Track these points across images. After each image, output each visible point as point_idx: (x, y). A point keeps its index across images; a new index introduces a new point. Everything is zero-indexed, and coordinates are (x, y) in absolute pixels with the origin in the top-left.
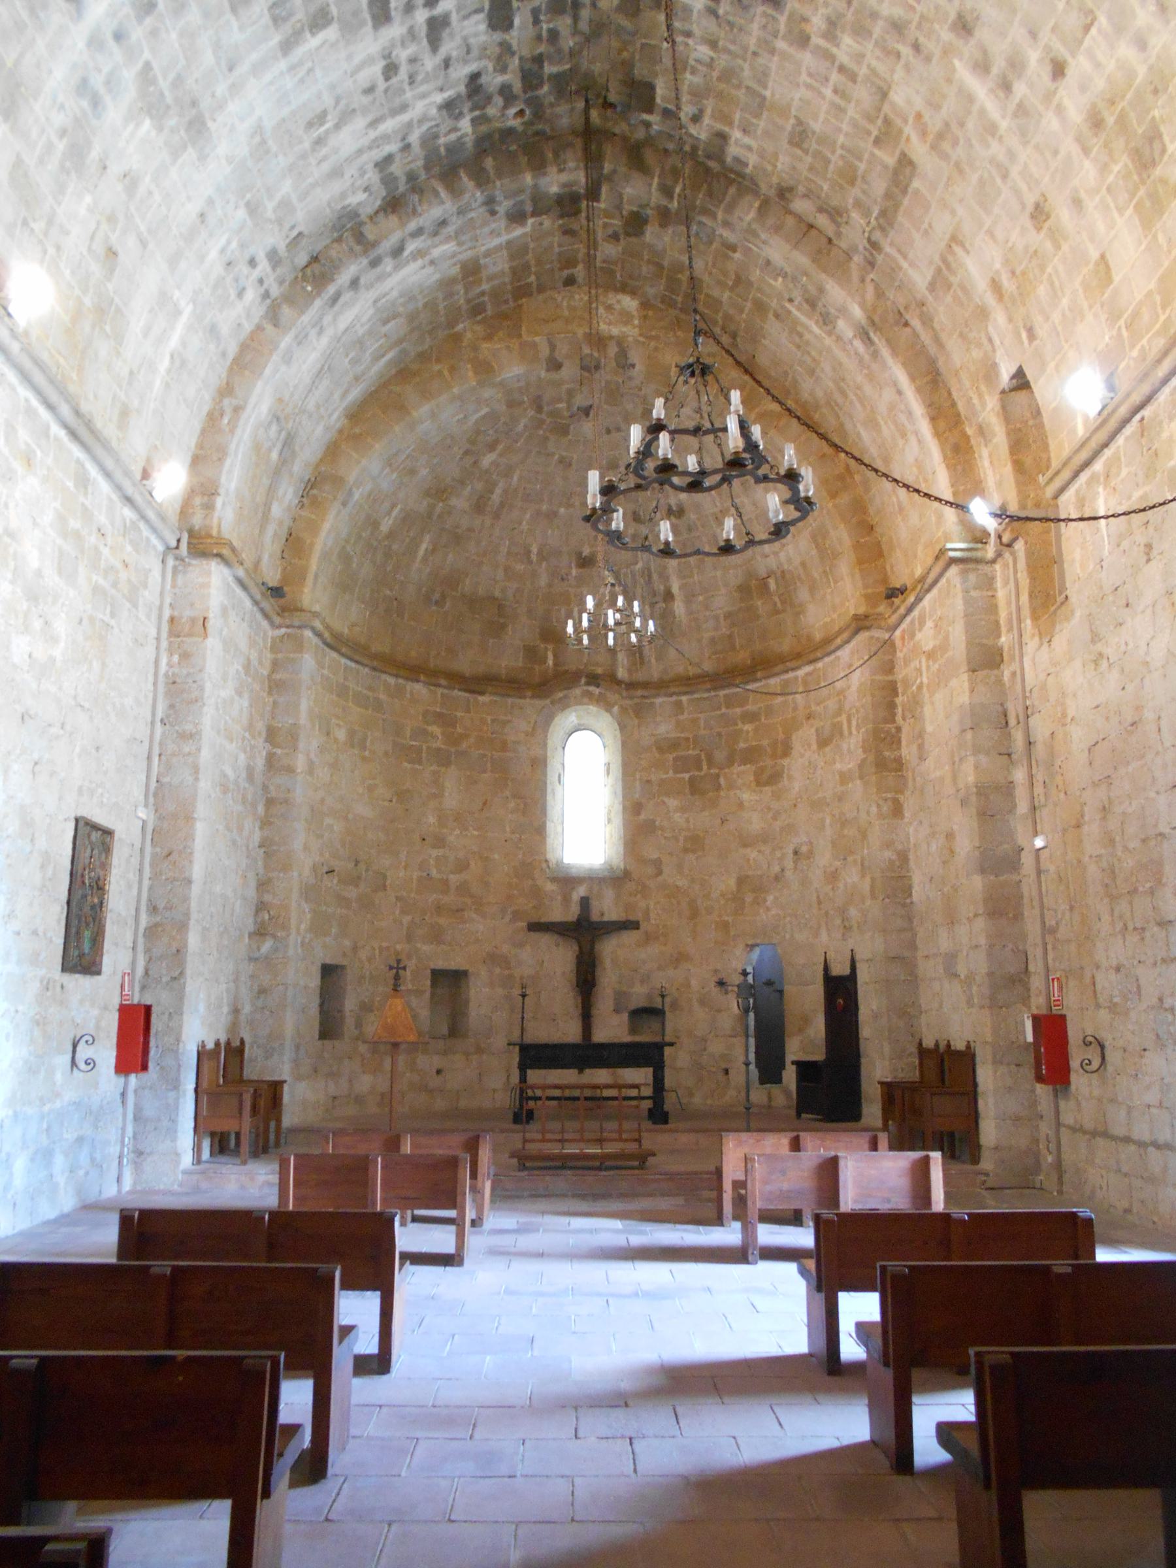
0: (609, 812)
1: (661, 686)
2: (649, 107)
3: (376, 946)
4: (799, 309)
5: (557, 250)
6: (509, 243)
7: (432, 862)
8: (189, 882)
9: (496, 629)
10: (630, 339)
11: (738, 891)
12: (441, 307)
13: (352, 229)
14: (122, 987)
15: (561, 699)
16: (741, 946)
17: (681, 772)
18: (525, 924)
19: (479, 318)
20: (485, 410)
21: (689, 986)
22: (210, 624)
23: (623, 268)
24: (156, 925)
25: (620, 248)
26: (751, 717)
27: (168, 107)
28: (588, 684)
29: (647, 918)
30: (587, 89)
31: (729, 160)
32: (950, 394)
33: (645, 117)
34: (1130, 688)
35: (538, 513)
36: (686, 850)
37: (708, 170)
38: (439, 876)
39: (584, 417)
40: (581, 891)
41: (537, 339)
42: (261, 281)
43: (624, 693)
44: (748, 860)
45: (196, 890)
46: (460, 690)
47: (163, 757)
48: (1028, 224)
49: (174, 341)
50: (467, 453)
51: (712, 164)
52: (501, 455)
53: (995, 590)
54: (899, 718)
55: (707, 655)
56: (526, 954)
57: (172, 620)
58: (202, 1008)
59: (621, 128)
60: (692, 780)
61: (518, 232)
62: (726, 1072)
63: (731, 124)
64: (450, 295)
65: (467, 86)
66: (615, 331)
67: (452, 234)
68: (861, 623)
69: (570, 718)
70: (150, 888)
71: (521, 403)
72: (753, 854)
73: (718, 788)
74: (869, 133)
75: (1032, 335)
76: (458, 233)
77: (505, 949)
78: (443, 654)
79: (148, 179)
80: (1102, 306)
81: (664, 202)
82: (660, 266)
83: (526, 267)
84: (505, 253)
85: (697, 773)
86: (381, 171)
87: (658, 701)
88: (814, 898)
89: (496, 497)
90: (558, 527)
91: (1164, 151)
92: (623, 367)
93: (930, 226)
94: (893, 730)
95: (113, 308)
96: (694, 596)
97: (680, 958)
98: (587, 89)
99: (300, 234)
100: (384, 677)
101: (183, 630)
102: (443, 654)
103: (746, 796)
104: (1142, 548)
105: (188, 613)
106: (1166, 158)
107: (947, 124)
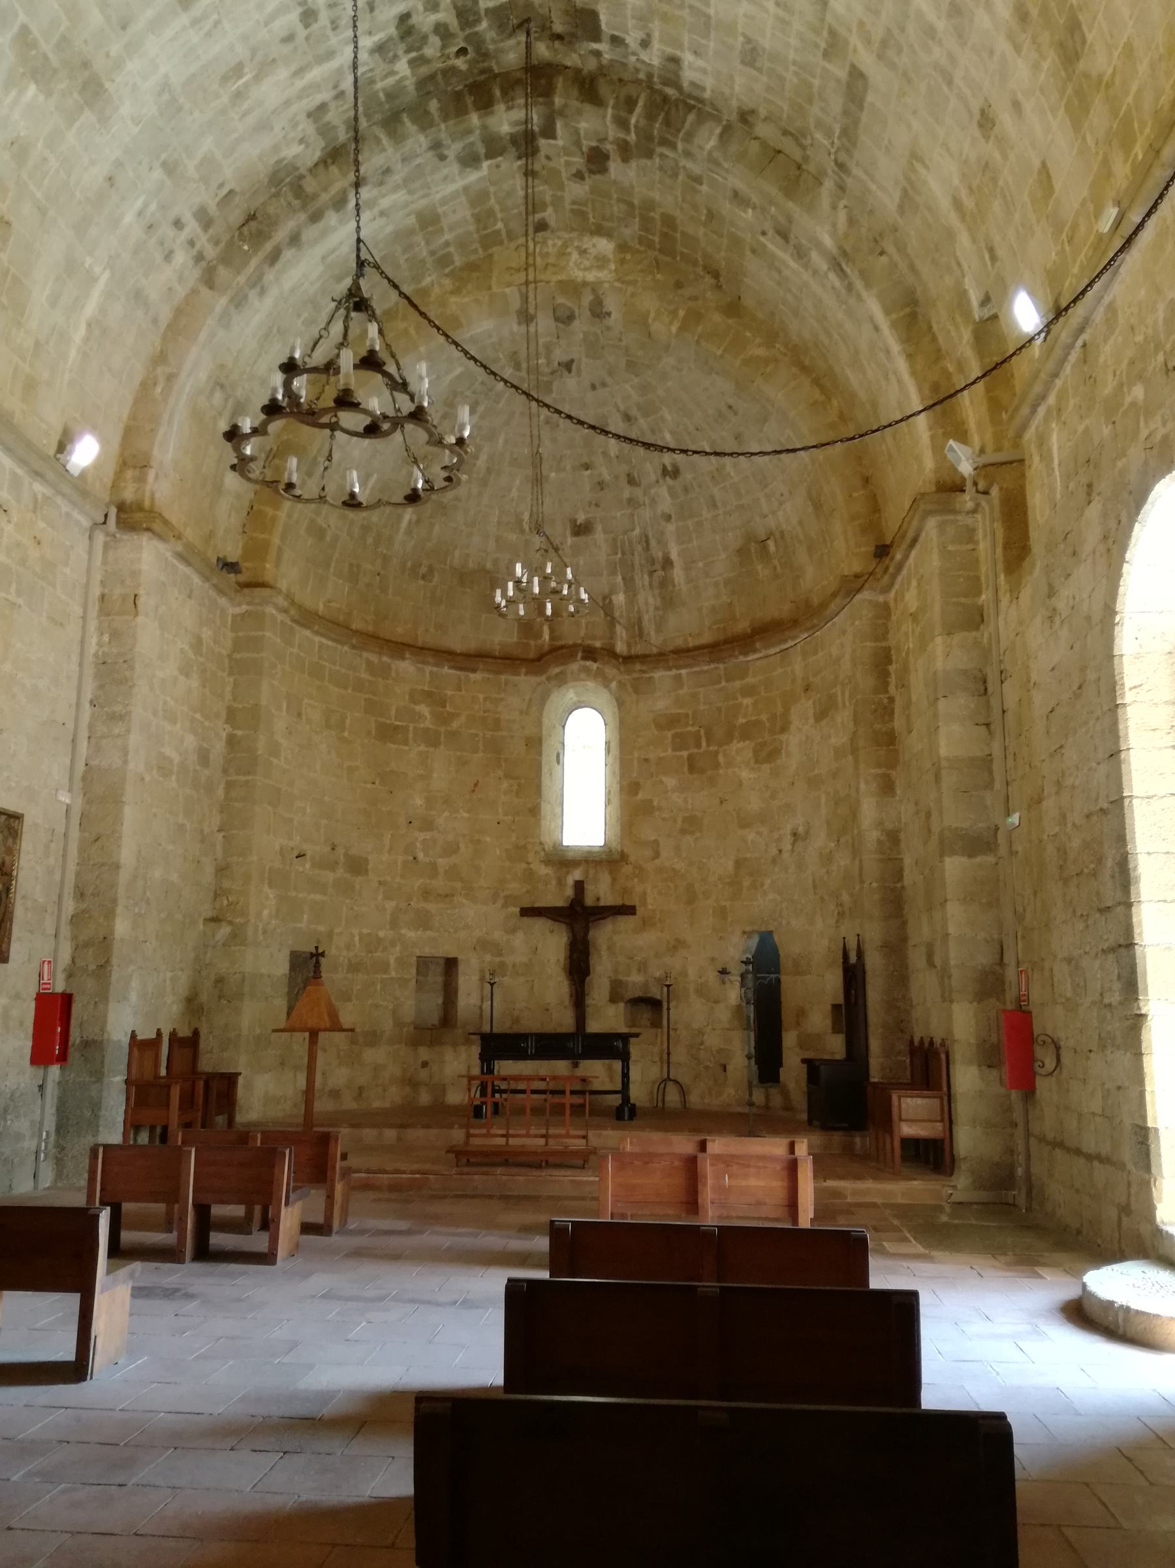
1: (660, 658)
2: (596, 36)
3: (355, 931)
6: (466, 189)
7: (418, 845)
8: (117, 867)
10: (606, 285)
12: (402, 261)
13: (291, 183)
14: (41, 975)
15: (557, 675)
17: (680, 750)
19: (447, 271)
21: (686, 975)
22: (141, 601)
23: (594, 210)
24: (84, 911)
25: (587, 187)
26: (749, 691)
27: (55, 71)
28: (584, 658)
29: (644, 903)
30: (528, 20)
31: (685, 85)
32: (930, 328)
33: (595, 46)
34: (1077, 647)
36: (683, 832)
37: (666, 99)
38: (427, 860)
39: (566, 373)
40: (577, 875)
41: (507, 290)
42: (192, 243)
43: (622, 668)
45: (124, 877)
46: (450, 668)
47: (93, 740)
48: (977, 133)
49: (90, 309)
51: (670, 91)
53: (977, 543)
54: (892, 689)
56: (518, 940)
57: (103, 597)
58: (133, 997)
59: (572, 60)
60: (691, 760)
61: (473, 176)
62: (725, 1068)
63: (681, 47)
64: (408, 248)
65: (397, 28)
66: (591, 277)
67: (400, 182)
68: (852, 585)
69: (570, 694)
70: (78, 874)
72: (751, 836)
73: (717, 766)
74: (817, 46)
75: (994, 258)
76: (406, 181)
77: (498, 935)
78: (432, 630)
79: (40, 145)
80: (1047, 217)
81: (622, 135)
82: (631, 205)
83: (490, 213)
84: (463, 198)
85: (696, 751)
86: (315, 122)
87: (658, 674)
88: (810, 881)
91: (1084, 41)
92: (598, 316)
93: (890, 141)
94: (886, 701)
95: (9, 278)
96: (693, 562)
97: (678, 945)
98: (528, 20)
99: (231, 192)
100: (365, 654)
101: (116, 606)
102: (432, 630)
103: (745, 774)
104: (1085, 488)
105: (118, 591)
106: (1087, 47)
107: (889, 30)
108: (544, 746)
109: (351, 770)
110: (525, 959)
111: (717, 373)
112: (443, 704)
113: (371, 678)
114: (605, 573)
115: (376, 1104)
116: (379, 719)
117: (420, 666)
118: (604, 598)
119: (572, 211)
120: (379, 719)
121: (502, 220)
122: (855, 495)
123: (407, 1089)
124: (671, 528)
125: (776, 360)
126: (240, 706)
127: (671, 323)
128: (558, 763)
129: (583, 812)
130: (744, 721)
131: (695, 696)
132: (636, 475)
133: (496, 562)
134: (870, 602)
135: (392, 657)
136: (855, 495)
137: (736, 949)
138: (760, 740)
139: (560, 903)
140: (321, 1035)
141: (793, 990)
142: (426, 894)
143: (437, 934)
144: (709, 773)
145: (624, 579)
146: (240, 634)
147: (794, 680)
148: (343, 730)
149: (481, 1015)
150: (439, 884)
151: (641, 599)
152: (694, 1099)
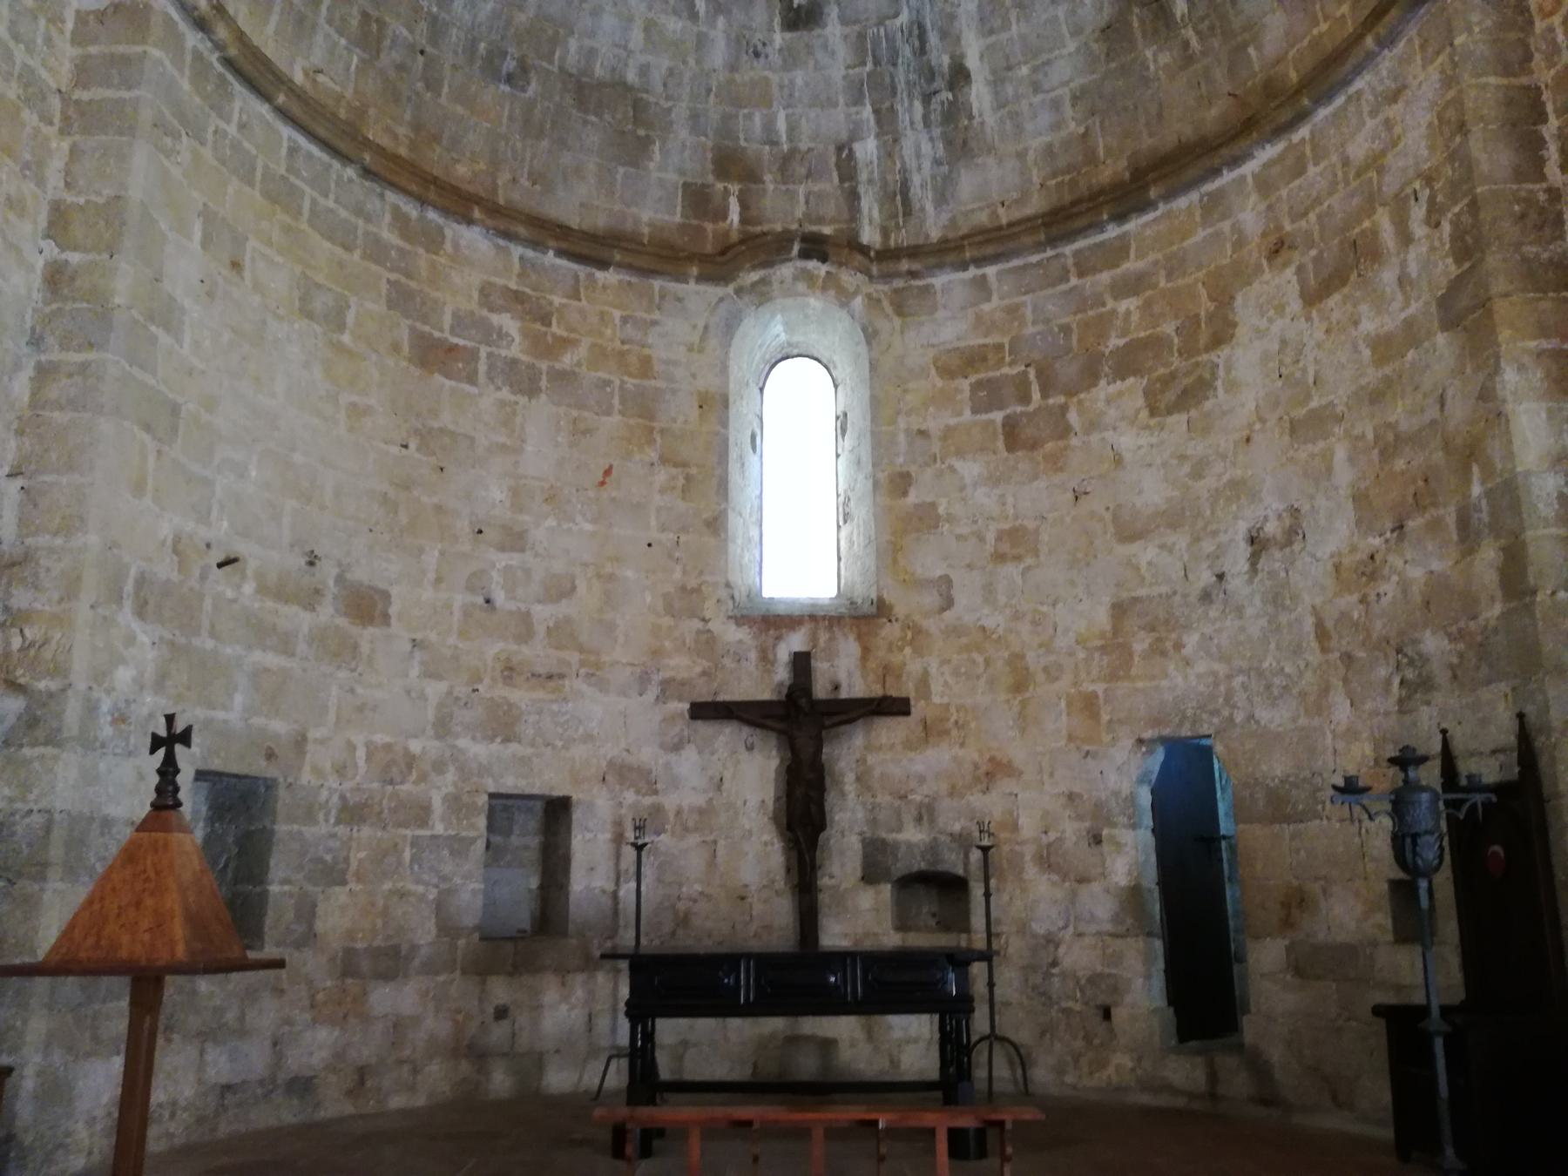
3: (359, 740)
7: (494, 574)
11: (1116, 631)
15: (754, 285)
16: (1128, 742)
17: (988, 410)
18: (687, 706)
21: (1015, 827)
28: (805, 255)
36: (999, 557)
38: (512, 606)
40: (796, 641)
46: (560, 253)
55: (1036, 180)
56: (688, 763)
62: (1107, 1014)
69: (772, 327)
72: (1146, 553)
73: (1065, 431)
77: (648, 755)
85: (1019, 409)
87: (939, 280)
88: (1309, 623)
94: (1542, 197)
96: (1009, 68)
97: (994, 771)
100: (392, 197)
103: (1127, 441)
108: (732, 411)
109: (356, 412)
110: (700, 800)
112: (545, 320)
113: (401, 243)
114: (841, 101)
115: (396, 1102)
116: (419, 325)
117: (501, 242)
118: (840, 149)
120: (419, 325)
123: (465, 1067)
126: (82, 200)
128: (754, 448)
129: (799, 532)
130: (1121, 342)
131: (1013, 311)
135: (446, 212)
137: (1126, 774)
138: (1162, 371)
139: (766, 695)
140: (172, 983)
141: (1262, 855)
142: (509, 672)
143: (529, 751)
144: (1050, 446)
145: (876, 112)
146: (93, 50)
147: (1240, 243)
148: (341, 327)
149: (616, 912)
150: (537, 654)
152: (1042, 1075)
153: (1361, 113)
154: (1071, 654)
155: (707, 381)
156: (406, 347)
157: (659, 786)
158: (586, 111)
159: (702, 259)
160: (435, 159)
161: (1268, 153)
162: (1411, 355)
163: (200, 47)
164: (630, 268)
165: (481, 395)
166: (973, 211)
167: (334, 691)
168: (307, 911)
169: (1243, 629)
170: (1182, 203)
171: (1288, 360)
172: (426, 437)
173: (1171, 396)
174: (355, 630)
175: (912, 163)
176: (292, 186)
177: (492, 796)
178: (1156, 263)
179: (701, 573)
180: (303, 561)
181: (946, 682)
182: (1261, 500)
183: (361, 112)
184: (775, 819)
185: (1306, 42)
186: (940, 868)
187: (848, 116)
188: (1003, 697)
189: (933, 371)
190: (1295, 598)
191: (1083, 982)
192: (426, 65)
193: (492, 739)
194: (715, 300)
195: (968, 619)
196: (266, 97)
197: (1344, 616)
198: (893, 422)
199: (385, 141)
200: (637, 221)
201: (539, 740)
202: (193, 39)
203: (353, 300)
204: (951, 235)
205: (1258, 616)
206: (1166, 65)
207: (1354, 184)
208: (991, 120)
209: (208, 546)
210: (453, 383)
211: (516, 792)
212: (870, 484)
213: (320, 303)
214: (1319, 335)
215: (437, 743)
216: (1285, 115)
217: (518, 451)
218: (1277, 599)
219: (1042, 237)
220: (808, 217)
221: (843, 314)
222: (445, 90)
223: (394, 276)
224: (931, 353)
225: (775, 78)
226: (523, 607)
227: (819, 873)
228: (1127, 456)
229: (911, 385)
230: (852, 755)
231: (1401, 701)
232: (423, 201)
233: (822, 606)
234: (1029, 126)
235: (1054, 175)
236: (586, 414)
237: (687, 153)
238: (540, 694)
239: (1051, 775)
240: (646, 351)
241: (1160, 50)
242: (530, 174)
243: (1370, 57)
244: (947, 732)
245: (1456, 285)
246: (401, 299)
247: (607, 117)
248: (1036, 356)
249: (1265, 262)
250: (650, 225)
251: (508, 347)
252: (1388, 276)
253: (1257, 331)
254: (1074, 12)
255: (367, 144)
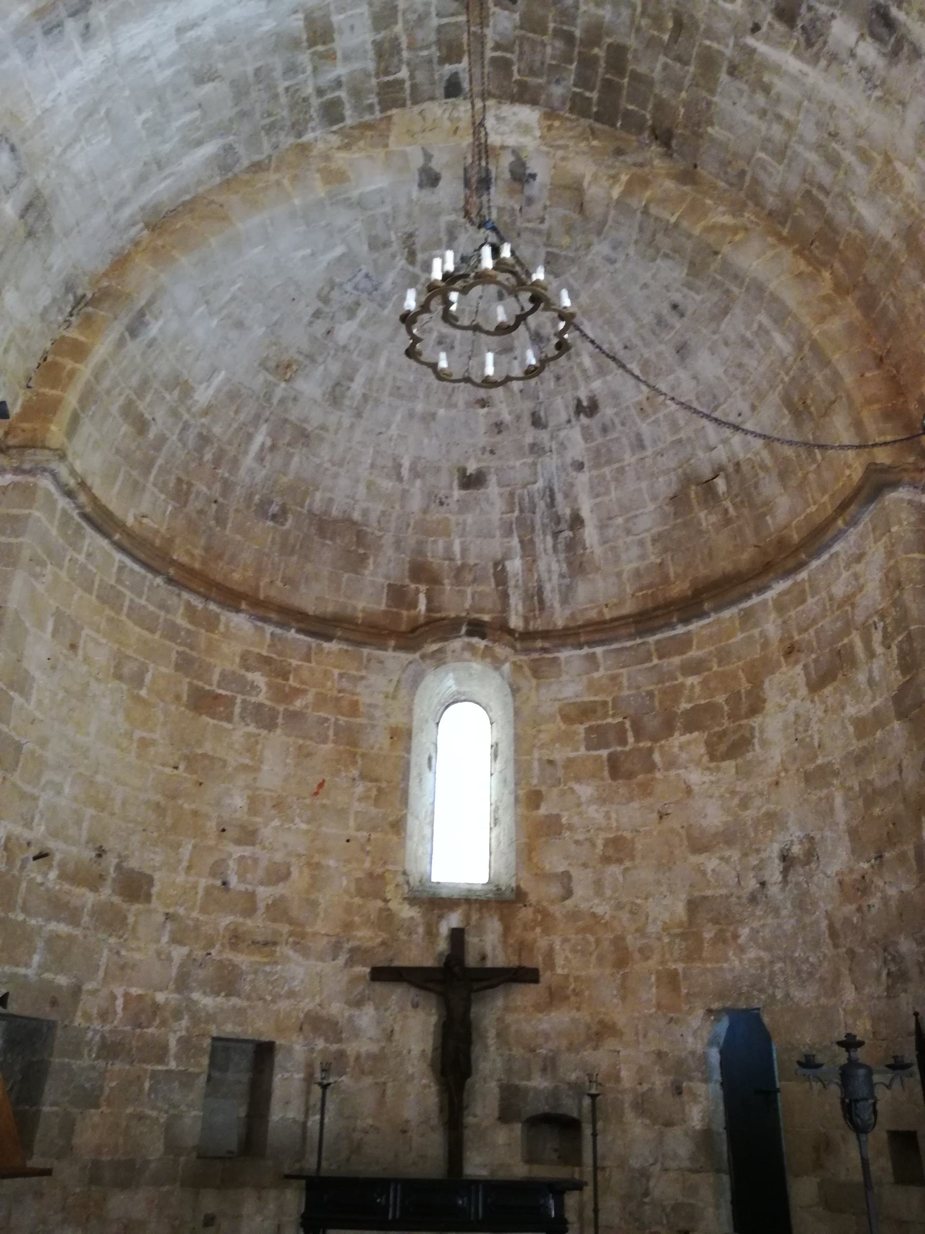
0: (496, 810)
3: (119, 991)
4: (767, 40)
5: (435, 22)
9: (355, 560)
16: (700, 1012)
17: (597, 748)
18: (368, 970)
19: (335, 128)
20: (339, 250)
21: (618, 1079)
23: (520, 59)
25: (517, 16)
28: (470, 634)
35: (411, 415)
36: (606, 860)
38: (242, 887)
40: (454, 920)
44: (704, 873)
46: (299, 631)
50: (317, 314)
52: (362, 326)
56: (366, 1017)
60: (613, 761)
64: (291, 69)
69: (446, 681)
71: (386, 244)
72: (711, 863)
73: (651, 767)
77: (336, 1008)
85: (619, 749)
87: (564, 655)
88: (824, 924)
89: (357, 386)
90: (437, 435)
96: (610, 518)
97: (603, 1031)
100: (186, 595)
102: (279, 583)
103: (695, 777)
108: (415, 742)
109: (144, 744)
110: (374, 1048)
111: (666, 256)
113: (189, 627)
116: (195, 682)
117: (260, 624)
118: (496, 564)
119: (494, 60)
120: (195, 682)
121: (408, 64)
122: (868, 375)
124: (583, 478)
125: (746, 229)
127: (611, 187)
128: (430, 766)
129: (461, 832)
130: (689, 706)
131: (613, 678)
132: (542, 414)
133: (365, 513)
134: (910, 502)
135: (222, 604)
136: (868, 375)
137: (698, 1037)
138: (717, 729)
139: (429, 963)
142: (236, 939)
143: (245, 1004)
144: (641, 777)
145: (521, 542)
147: (765, 645)
150: (257, 925)
151: (542, 565)
153: (839, 566)
154: (659, 939)
155: (397, 719)
156: (185, 698)
157: (344, 1035)
158: (324, 538)
159: (399, 635)
160: (219, 570)
161: (781, 586)
162: (879, 734)
163: (67, 507)
164: (347, 640)
165: (234, 729)
166: (586, 609)
167: (106, 953)
168: (68, 1128)
169: (779, 926)
170: (726, 614)
171: (801, 729)
172: (191, 761)
173: (723, 748)
174: (125, 906)
175: (545, 576)
176: (120, 592)
177: (215, 1039)
178: (710, 653)
179: (385, 863)
180: (93, 854)
181: (566, 957)
182: (788, 829)
183: (171, 540)
184: (432, 1065)
185: (802, 517)
186: (561, 1111)
187: (502, 543)
188: (608, 971)
189: (559, 718)
190: (814, 904)
191: (668, 1210)
192: (217, 510)
193: (218, 994)
194: (406, 662)
195: (583, 906)
196: (106, 535)
197: (847, 920)
198: (529, 752)
199: (185, 559)
200: (355, 608)
201: (254, 995)
202: (63, 502)
203: (151, 666)
204: (572, 624)
205: (790, 917)
206: (713, 524)
207: (837, 613)
208: (598, 551)
209: (29, 844)
210: (215, 722)
211: (233, 1036)
212: (512, 798)
213: (128, 669)
214: (820, 713)
215: (176, 996)
216: (790, 563)
217: (257, 769)
218: (803, 904)
219: (633, 630)
220: (473, 608)
221: (496, 675)
222: (229, 525)
223: (181, 649)
224: (557, 705)
225: (453, 518)
226: (250, 888)
227: (465, 1113)
228: (696, 788)
229: (543, 727)
230: (494, 1013)
231: (888, 989)
232: (207, 598)
233: (475, 891)
234: (624, 557)
235: (641, 589)
236: (309, 742)
237: (392, 565)
238: (256, 958)
239: (645, 1036)
240: (356, 698)
241: (710, 513)
242: (283, 578)
243: (841, 533)
244: (567, 998)
245: (903, 689)
246: (185, 664)
247: (338, 541)
248: (631, 712)
249: (782, 659)
250: (363, 611)
251: (257, 695)
252: (861, 678)
253: (780, 706)
254: (652, 487)
255: (173, 562)
